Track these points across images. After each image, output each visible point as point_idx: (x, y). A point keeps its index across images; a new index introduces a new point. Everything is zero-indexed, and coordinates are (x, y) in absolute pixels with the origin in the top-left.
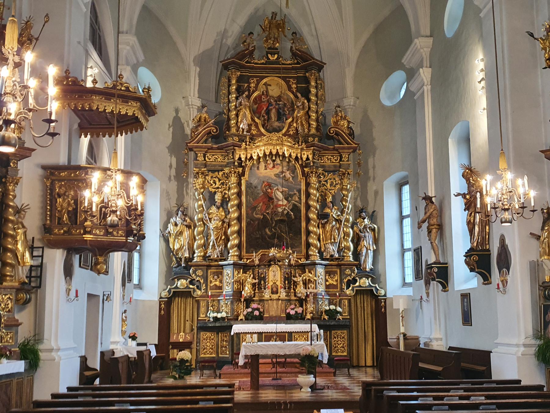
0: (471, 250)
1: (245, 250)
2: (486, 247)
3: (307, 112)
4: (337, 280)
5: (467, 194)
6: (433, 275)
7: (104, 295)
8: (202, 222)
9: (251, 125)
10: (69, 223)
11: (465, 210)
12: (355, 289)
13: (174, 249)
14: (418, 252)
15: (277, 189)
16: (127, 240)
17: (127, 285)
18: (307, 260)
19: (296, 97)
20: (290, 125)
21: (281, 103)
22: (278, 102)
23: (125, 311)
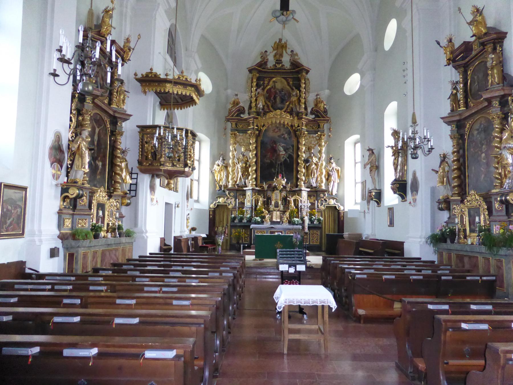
0: (395, 180)
5: (394, 146)
7: (175, 204)
10: (152, 159)
11: (392, 156)
12: (325, 206)
13: (217, 180)
14: (364, 183)
15: (280, 145)
16: (184, 169)
17: (190, 199)
18: (296, 188)
19: (293, 89)
20: (288, 106)
23: (188, 214)
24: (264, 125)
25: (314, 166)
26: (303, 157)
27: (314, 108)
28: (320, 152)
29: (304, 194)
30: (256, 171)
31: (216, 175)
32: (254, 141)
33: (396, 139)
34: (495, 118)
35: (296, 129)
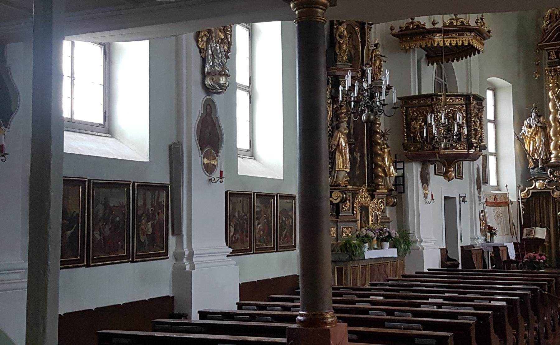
7: (460, 197)
8: (401, 183)
13: (530, 151)
16: (468, 152)
17: (483, 187)
31: (526, 143)
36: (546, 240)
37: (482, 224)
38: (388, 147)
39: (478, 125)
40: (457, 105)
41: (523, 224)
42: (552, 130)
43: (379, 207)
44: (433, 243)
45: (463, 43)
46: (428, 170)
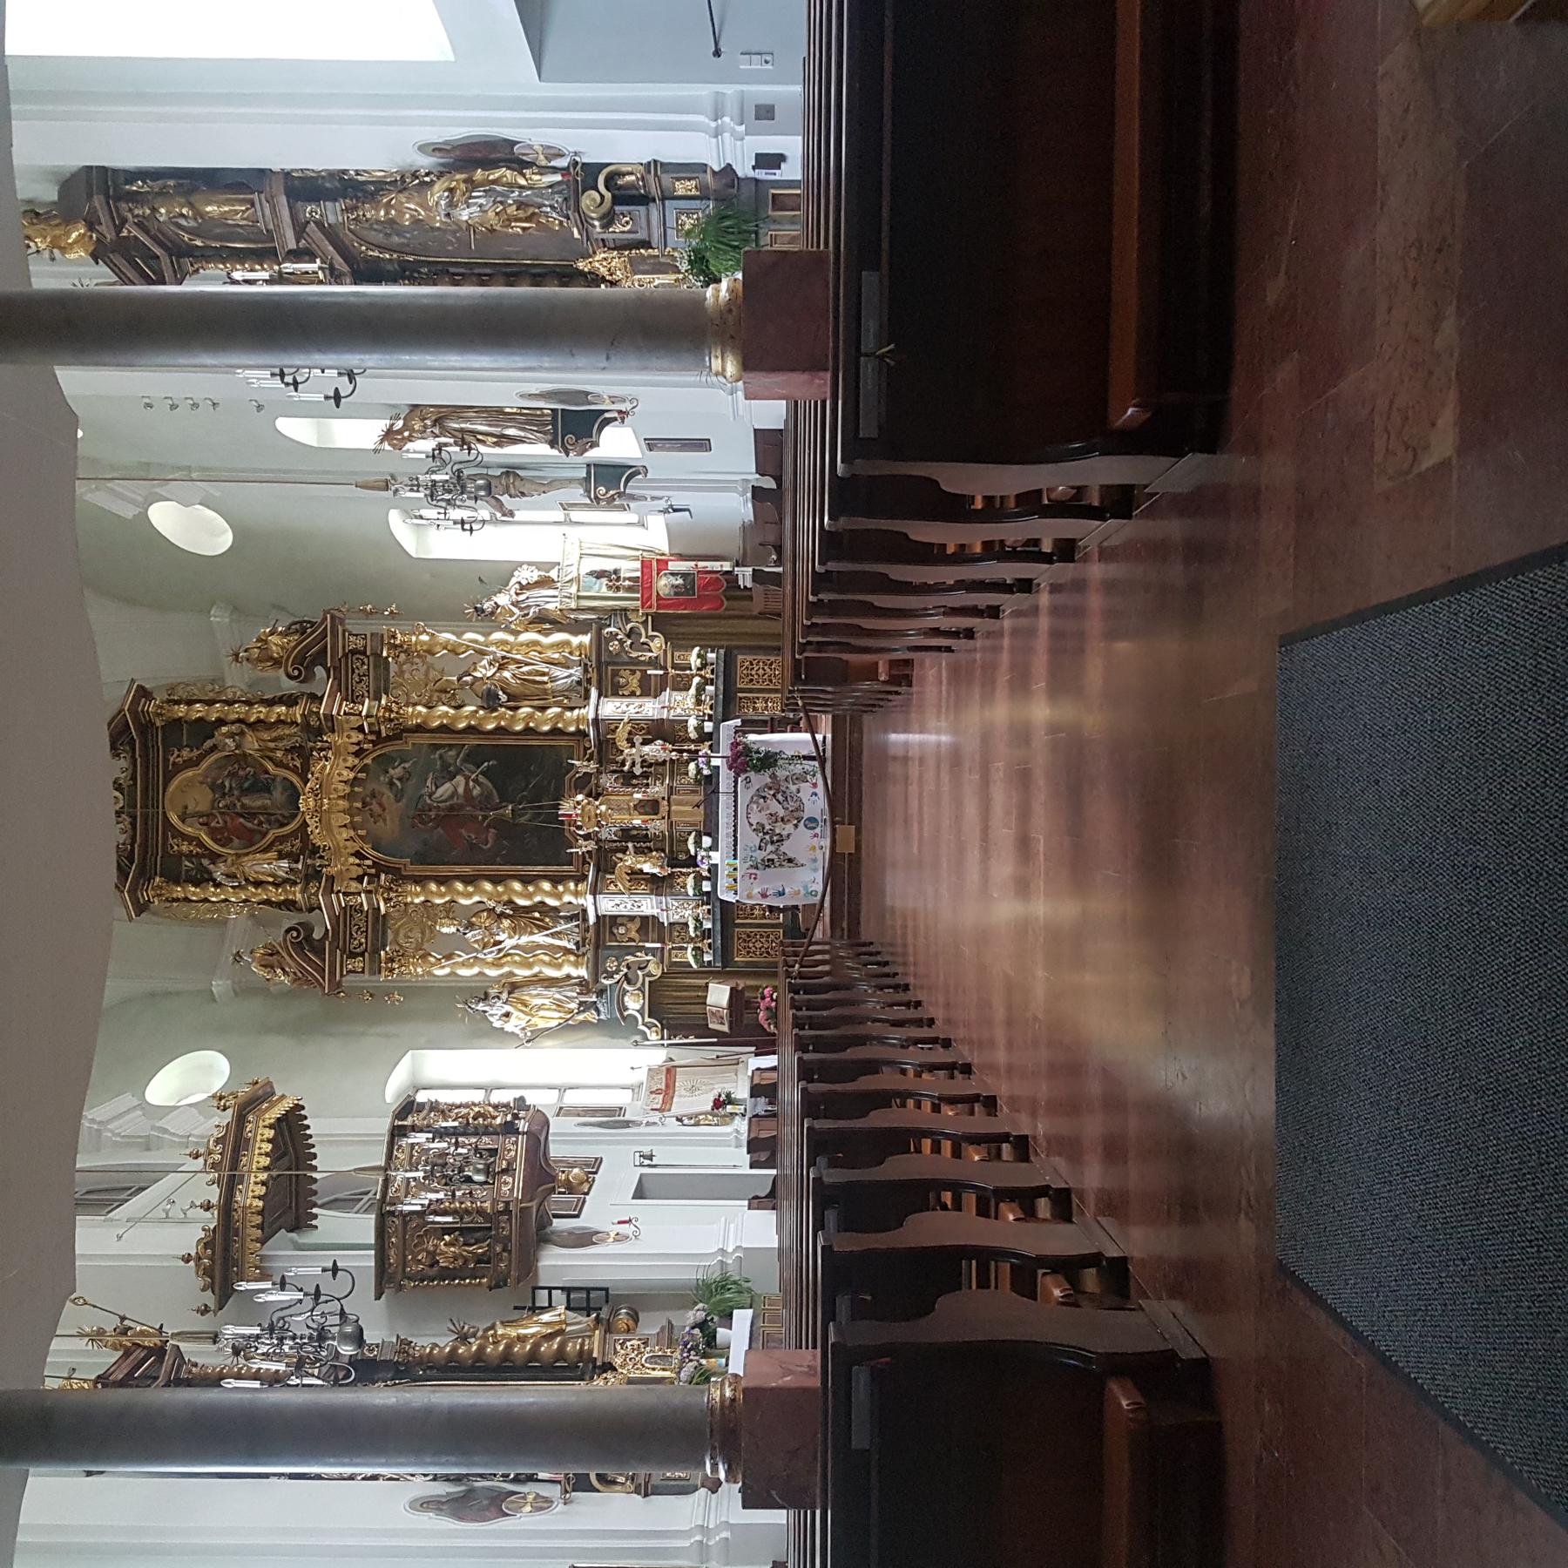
1: (566, 868)
2: (547, 415)
3: (250, 725)
4: (631, 670)
6: (613, 496)
7: (641, 1165)
9: (280, 852)
12: (650, 633)
15: (430, 796)
16: (524, 1133)
18: (588, 735)
19: (214, 748)
20: (279, 764)
21: (227, 784)
22: (226, 790)
24: (358, 855)
25: (507, 674)
26: (476, 712)
27: (290, 670)
28: (454, 651)
29: (611, 708)
30: (526, 880)
31: (542, 1024)
32: (418, 889)
33: (415, 435)
34: (358, 215)
35: (369, 737)
36: (734, 985)
37: (707, 1122)
38: (493, 1327)
39: (466, 1111)
40: (412, 1156)
41: (715, 1040)
42: (517, 971)
43: (633, 1350)
44: (732, 1226)
45: (269, 1141)
46: (562, 1232)
